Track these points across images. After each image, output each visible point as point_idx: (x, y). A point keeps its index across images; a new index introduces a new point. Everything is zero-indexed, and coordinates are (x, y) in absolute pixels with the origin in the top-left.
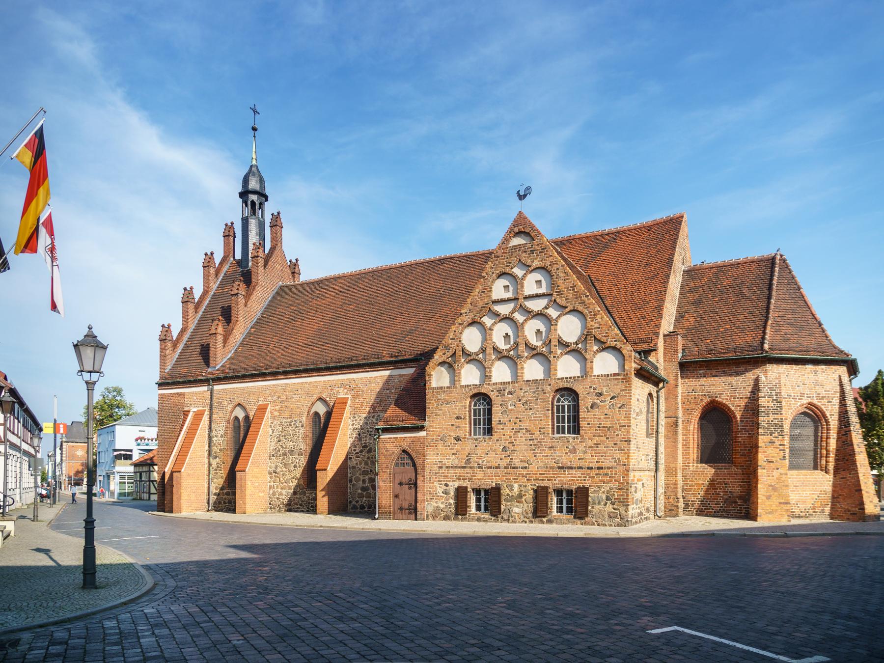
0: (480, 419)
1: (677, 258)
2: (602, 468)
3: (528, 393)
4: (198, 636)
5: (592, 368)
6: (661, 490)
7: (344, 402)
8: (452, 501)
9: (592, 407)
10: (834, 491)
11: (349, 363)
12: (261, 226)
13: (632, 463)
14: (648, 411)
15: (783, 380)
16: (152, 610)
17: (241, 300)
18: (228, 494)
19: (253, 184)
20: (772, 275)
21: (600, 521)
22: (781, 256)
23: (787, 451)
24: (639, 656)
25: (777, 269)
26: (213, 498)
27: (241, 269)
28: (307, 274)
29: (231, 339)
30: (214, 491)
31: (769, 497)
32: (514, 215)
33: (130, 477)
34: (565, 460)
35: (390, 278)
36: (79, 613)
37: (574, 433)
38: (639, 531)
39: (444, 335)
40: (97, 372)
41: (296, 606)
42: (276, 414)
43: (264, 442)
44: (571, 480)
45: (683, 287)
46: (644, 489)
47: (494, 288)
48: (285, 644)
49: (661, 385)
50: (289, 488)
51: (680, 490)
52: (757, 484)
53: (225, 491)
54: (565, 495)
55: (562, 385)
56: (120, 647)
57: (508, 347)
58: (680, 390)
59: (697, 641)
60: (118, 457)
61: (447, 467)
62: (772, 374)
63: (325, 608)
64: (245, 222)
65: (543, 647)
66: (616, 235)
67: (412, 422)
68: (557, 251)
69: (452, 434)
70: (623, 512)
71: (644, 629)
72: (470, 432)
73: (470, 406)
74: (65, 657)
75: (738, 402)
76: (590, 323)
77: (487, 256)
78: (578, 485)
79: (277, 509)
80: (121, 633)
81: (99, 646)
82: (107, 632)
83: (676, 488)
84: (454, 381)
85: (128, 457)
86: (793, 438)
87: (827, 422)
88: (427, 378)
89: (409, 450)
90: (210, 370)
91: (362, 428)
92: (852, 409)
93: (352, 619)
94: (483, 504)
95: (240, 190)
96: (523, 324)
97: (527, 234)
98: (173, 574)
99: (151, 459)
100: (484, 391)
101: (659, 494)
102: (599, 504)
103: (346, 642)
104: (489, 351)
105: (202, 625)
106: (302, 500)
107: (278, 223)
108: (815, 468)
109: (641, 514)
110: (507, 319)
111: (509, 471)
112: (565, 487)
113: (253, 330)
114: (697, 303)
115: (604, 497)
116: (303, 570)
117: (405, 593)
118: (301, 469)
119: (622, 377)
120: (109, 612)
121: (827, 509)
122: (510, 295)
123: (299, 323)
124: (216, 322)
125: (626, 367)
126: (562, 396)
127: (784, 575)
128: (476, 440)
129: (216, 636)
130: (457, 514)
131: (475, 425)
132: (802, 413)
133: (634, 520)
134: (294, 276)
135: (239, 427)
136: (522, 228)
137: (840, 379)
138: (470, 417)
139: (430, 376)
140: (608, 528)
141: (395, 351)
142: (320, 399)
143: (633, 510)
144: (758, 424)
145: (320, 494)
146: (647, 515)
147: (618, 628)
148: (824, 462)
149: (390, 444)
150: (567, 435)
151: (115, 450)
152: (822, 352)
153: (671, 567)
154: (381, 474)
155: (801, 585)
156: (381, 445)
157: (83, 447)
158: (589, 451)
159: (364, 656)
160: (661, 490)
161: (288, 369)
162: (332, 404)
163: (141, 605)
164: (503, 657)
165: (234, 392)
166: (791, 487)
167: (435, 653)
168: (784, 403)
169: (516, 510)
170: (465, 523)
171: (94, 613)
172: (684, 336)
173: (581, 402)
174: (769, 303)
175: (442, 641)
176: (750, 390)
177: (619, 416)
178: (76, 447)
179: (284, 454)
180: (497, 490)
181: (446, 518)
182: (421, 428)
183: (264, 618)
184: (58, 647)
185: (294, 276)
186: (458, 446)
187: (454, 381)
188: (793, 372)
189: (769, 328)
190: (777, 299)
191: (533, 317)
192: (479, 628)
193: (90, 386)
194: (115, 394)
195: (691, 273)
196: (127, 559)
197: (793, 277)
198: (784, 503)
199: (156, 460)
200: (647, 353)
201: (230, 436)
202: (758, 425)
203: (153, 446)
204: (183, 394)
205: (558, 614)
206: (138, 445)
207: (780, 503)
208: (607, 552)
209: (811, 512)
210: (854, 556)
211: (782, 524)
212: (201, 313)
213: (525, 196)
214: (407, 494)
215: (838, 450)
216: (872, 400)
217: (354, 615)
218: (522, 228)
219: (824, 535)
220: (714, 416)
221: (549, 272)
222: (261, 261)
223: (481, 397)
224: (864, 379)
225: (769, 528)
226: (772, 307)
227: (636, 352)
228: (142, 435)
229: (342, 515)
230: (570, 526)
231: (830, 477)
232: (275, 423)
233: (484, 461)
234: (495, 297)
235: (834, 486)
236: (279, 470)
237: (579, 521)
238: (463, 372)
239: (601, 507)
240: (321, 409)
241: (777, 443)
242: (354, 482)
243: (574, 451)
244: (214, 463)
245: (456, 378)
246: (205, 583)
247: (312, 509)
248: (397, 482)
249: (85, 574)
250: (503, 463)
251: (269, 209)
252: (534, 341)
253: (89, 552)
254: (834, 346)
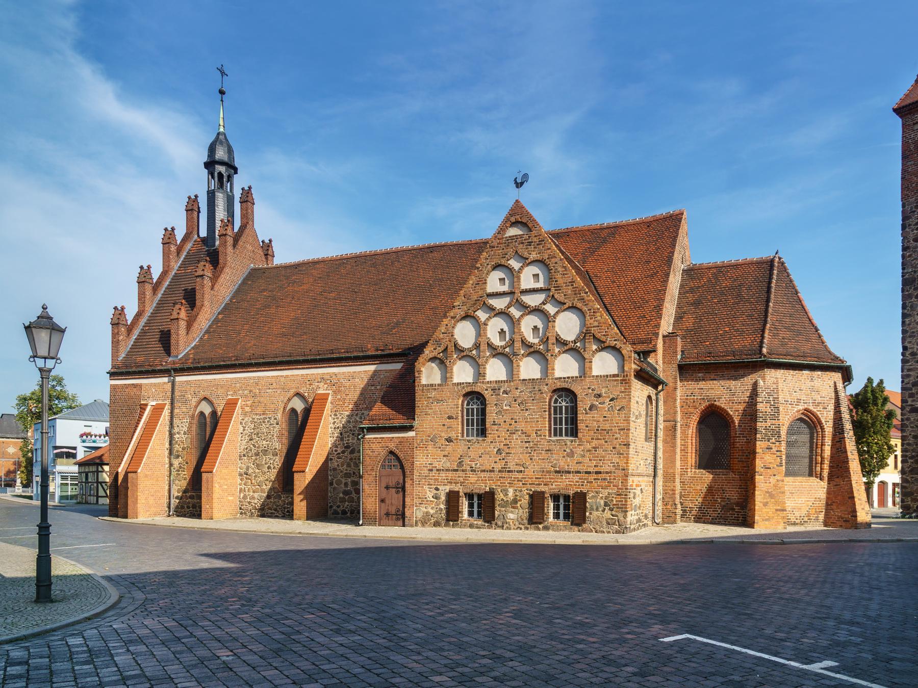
0: (473, 420)
1: (677, 257)
2: (600, 473)
3: (524, 393)
4: (181, 652)
5: (591, 368)
6: (659, 496)
7: (324, 398)
8: (442, 506)
9: (590, 409)
10: (828, 498)
11: (329, 356)
12: (230, 201)
13: (631, 467)
14: (647, 414)
15: (780, 386)
16: (122, 625)
17: (207, 282)
18: (192, 497)
19: (221, 154)
20: (771, 278)
21: (598, 527)
22: (780, 258)
23: (784, 457)
24: (654, 665)
25: (775, 272)
26: (175, 502)
27: (207, 251)
28: (282, 257)
29: (196, 325)
30: (176, 494)
31: (765, 504)
32: (510, 204)
33: (73, 478)
34: (563, 464)
35: (374, 265)
36: (37, 630)
37: (572, 435)
38: (637, 538)
39: (436, 328)
40: (53, 358)
41: (287, 618)
42: (248, 409)
43: (233, 441)
44: (568, 485)
45: (682, 286)
46: (642, 495)
47: (489, 280)
48: (281, 659)
49: (660, 388)
50: (263, 491)
51: (678, 496)
52: (754, 490)
53: (188, 495)
54: (562, 500)
55: (559, 385)
56: (92, 666)
57: (503, 343)
58: (679, 393)
59: (711, 649)
60: (59, 456)
61: (438, 470)
62: (771, 378)
63: (318, 620)
64: (211, 196)
65: (557, 657)
66: (615, 229)
67: (400, 421)
68: (555, 243)
69: (443, 434)
70: (622, 518)
71: (656, 637)
72: (463, 433)
73: (462, 405)
74: (28, 679)
75: (736, 406)
76: (589, 321)
77: (481, 246)
78: (576, 490)
79: (249, 514)
80: (90, 651)
81: (67, 665)
82: (73, 650)
83: (674, 494)
84: (446, 378)
85: (74, 456)
86: (789, 444)
87: (822, 429)
88: (417, 375)
89: (397, 452)
90: (170, 359)
91: (344, 427)
92: (846, 416)
93: (351, 631)
94: (476, 509)
95: (205, 159)
96: (519, 320)
97: (524, 225)
98: (140, 585)
99: (100, 457)
100: (477, 389)
101: (657, 500)
102: (597, 510)
103: (348, 656)
104: (484, 347)
105: (183, 640)
106: (277, 504)
107: (249, 199)
108: (810, 475)
109: (639, 520)
110: (503, 314)
111: (504, 474)
112: (563, 492)
113: (220, 316)
114: (696, 304)
115: (602, 502)
116: (288, 580)
117: (403, 603)
118: (276, 471)
119: (622, 378)
120: (72, 628)
121: (822, 517)
122: (505, 288)
123: (273, 310)
124: (177, 306)
125: (626, 369)
126: (560, 397)
127: (786, 582)
128: (469, 441)
129: (202, 652)
130: (448, 520)
131: (468, 425)
132: (798, 419)
133: (632, 527)
134: (267, 259)
135: (205, 424)
136: (519, 217)
137: (835, 386)
138: (462, 417)
139: (420, 372)
140: (606, 534)
141: (380, 344)
142: (298, 394)
143: (631, 517)
144: (756, 429)
145: (297, 498)
146: (646, 522)
147: (629, 636)
148: (818, 469)
149: (376, 445)
150: (564, 438)
151: (56, 448)
152: (818, 358)
153: (675, 574)
154: (366, 476)
155: (803, 592)
156: (367, 446)
157: (15, 443)
158: (587, 454)
159: (369, 670)
160: (659, 496)
161: (262, 361)
162: (310, 400)
163: (107, 620)
164: (518, 669)
165: (199, 384)
166: (787, 494)
167: (445, 666)
168: (781, 409)
169: (511, 516)
170: (457, 530)
171: (54, 630)
172: (684, 337)
173: (580, 404)
174: (767, 306)
175: (451, 653)
176: (748, 394)
177: (619, 419)
178: (7, 443)
179: (257, 454)
180: (491, 495)
181: (437, 524)
182: (410, 428)
183: (252, 632)
184: (18, 668)
185: (267, 259)
186: (449, 448)
187: (446, 378)
188: (790, 377)
189: (767, 332)
190: (776, 303)
191: (530, 313)
192: (487, 639)
193: (44, 373)
194: (55, 383)
195: (691, 273)
196: (83, 570)
197: (791, 281)
198: (780, 510)
199: (106, 459)
200: (646, 353)
201: (194, 433)
202: (755, 431)
203: (103, 443)
204: (140, 386)
205: (567, 623)
206: (84, 441)
207: (777, 510)
208: (608, 560)
209: (806, 519)
210: (851, 563)
211: (779, 531)
212: (160, 295)
213: (522, 184)
214: (394, 498)
215: (832, 456)
216: (862, 408)
217: (353, 628)
218: (519, 217)
219: (818, 542)
220: (713, 420)
221: (547, 266)
222: (230, 241)
223: (474, 396)
224: (856, 387)
225: (765, 535)
226: (770, 310)
227: (636, 352)
228: (87, 430)
229: (321, 521)
230: (567, 532)
231: (824, 484)
232: (246, 419)
234: (489, 290)
235: (828, 493)
236: (251, 471)
237: (576, 528)
238: (455, 368)
239: (599, 513)
240: (299, 405)
241: (774, 449)
242: (335, 485)
243: (571, 454)
244: (176, 463)
245: (448, 375)
246: (179, 594)
247: (288, 514)
248: (384, 485)
249: (38, 586)
250: (498, 467)
251: (239, 183)
252: (531, 338)
253: (44, 561)
254: (830, 352)
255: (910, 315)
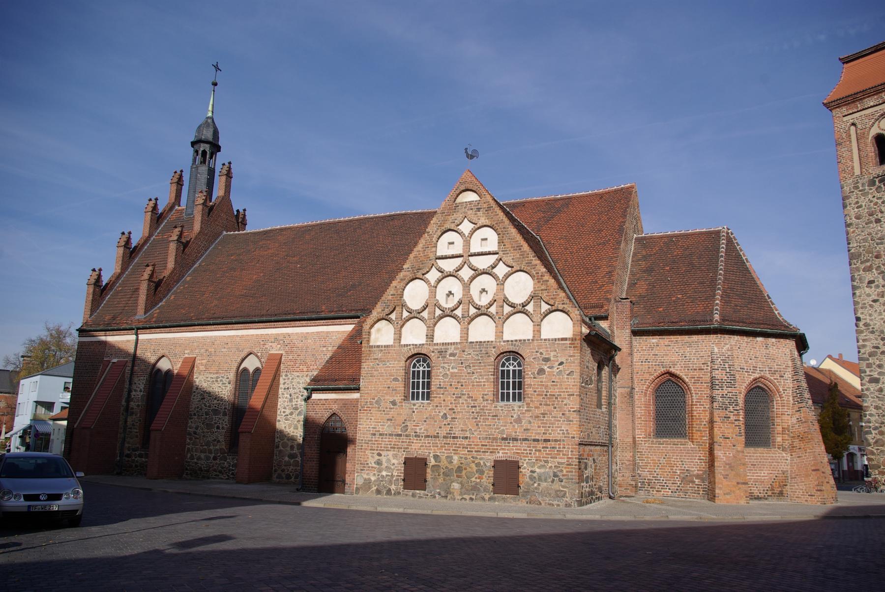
2: (549, 441)
34: (509, 430)
61: (380, 435)
102: (546, 480)
114: (649, 270)
165: (159, 342)
233: (421, 429)
242: (281, 448)
250: (443, 432)
251: (221, 158)
255: (859, 287)
